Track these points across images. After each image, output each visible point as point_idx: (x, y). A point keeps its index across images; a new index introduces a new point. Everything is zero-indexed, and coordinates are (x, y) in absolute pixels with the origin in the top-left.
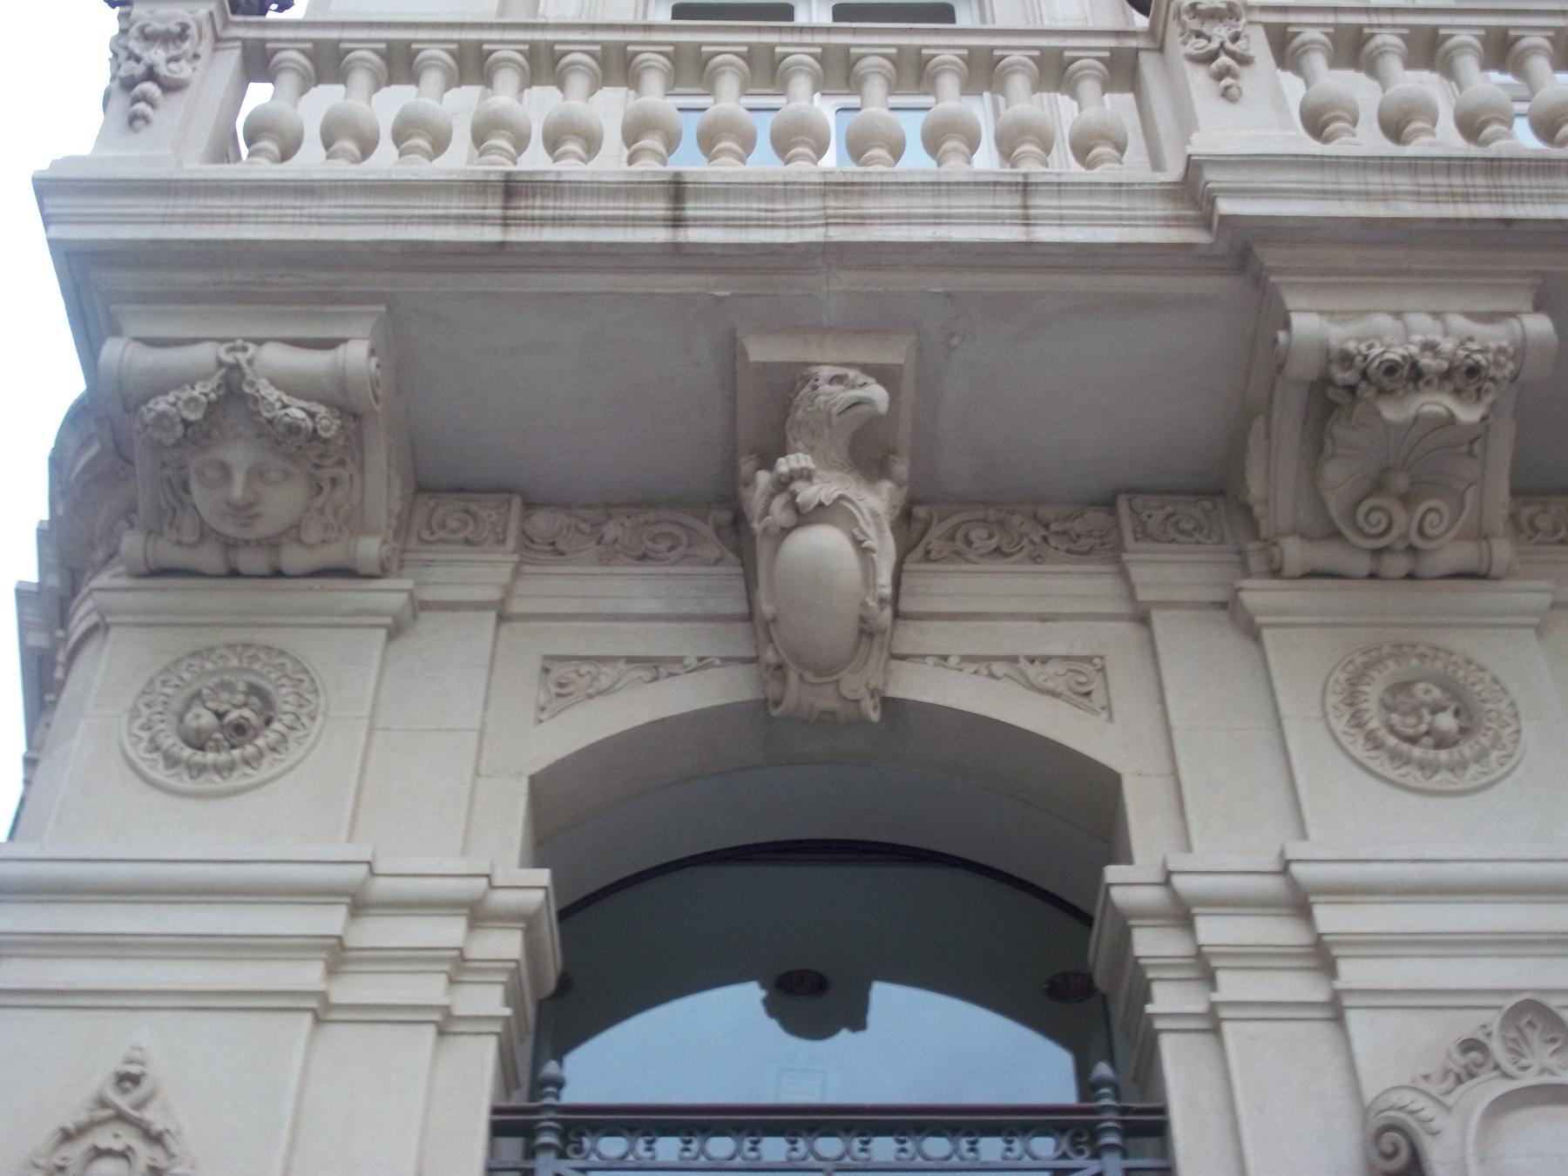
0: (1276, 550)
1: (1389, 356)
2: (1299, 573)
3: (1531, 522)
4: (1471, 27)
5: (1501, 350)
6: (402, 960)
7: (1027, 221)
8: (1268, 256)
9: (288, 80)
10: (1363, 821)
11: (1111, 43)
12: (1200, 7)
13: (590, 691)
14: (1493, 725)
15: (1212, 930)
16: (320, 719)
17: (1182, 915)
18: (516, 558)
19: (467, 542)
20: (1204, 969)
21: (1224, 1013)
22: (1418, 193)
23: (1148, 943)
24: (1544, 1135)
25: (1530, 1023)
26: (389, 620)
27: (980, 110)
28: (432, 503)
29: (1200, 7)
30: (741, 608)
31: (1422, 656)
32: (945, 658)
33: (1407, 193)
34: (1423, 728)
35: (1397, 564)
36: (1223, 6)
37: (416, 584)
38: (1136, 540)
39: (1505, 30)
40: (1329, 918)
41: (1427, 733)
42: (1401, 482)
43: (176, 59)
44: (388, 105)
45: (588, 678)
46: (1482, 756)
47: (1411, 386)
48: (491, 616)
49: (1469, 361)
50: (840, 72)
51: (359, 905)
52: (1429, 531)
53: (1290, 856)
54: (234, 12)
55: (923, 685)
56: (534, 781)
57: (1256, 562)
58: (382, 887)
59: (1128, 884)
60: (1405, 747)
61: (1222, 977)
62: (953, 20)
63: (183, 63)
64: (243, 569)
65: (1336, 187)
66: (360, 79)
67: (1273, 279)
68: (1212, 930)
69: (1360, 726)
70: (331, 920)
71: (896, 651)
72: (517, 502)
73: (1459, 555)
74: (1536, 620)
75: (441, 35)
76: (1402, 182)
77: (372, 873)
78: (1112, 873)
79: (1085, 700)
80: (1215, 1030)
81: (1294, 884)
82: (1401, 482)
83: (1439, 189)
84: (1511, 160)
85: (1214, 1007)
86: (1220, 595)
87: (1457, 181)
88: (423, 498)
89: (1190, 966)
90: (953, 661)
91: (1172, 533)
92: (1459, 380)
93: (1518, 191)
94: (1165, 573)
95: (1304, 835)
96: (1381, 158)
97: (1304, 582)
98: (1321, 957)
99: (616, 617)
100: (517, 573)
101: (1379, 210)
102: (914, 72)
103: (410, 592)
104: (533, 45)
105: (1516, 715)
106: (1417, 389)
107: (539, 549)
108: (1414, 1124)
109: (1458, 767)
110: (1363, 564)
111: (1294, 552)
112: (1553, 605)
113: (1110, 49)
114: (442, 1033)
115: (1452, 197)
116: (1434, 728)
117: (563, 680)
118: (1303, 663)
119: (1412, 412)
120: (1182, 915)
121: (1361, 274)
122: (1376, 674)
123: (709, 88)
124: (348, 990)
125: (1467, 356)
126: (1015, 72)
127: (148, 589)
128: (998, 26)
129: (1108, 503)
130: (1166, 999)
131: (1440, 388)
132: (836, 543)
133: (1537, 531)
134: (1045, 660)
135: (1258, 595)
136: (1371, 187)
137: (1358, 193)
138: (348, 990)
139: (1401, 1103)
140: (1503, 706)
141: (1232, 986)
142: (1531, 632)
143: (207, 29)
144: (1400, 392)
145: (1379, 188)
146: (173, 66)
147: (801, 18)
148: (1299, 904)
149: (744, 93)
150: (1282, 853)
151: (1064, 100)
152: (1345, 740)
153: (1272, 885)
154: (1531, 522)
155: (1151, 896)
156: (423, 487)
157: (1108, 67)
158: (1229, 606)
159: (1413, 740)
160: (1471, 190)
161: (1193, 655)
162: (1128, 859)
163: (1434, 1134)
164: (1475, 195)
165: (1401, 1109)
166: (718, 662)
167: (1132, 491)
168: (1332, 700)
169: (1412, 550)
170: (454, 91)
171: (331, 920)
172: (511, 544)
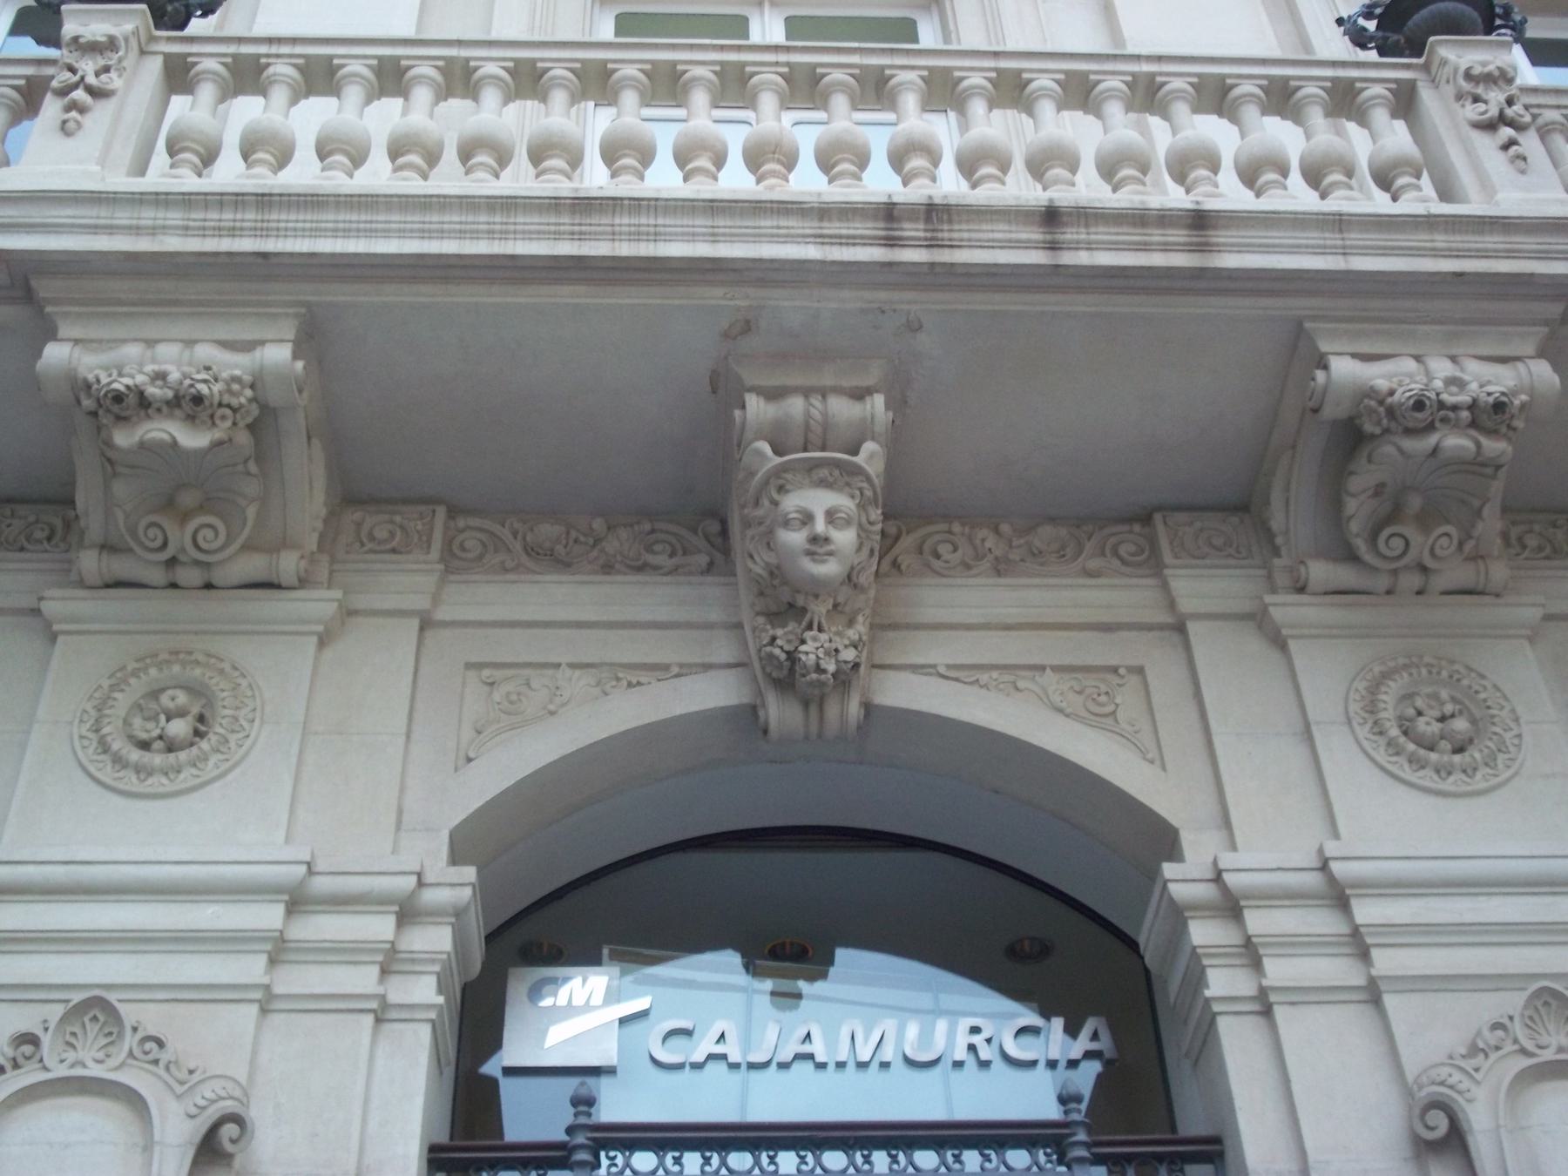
0: (1302, 569)
1: (115, 386)
3: (1520, 539)
4: (365, 57)
5: (236, 379)
6: (1309, 944)
7: (1053, 247)
8: (44, 288)
9: (280, 95)
10: (1389, 821)
11: (29, 71)
12: (82, 40)
14: (1497, 729)
19: (394, 551)
20: (1251, 954)
21: (1273, 998)
22: (187, 228)
23: (1203, 933)
24: (1562, 1109)
25: (1546, 1003)
26: (320, 628)
27: (943, 130)
28: (357, 516)
29: (82, 40)
31: (159, 666)
33: (176, 227)
34: (156, 732)
35: (1412, 580)
36: (103, 39)
39: (396, 60)
40: (1367, 912)
41: (160, 737)
42: (1415, 503)
43: (107, 69)
44: (384, 118)
46: (1490, 762)
47: (142, 413)
48: (415, 623)
49: (193, 390)
50: (805, 88)
51: (297, 902)
52: (1438, 551)
54: (157, 27)
55: (901, 692)
57: (1282, 579)
58: (321, 885)
59: (1183, 879)
60: (1422, 752)
61: (1268, 963)
62: (915, 40)
63: (113, 74)
64: (181, 582)
65: (109, 222)
66: (353, 93)
67: (49, 309)
68: (1258, 921)
70: (270, 916)
71: (877, 661)
72: (441, 512)
73: (1461, 574)
74: (1529, 632)
75: (495, 53)
76: (175, 217)
78: (1169, 869)
80: (1267, 1012)
81: (1332, 880)
82: (1415, 503)
83: (223, 224)
84: (281, 195)
85: (1263, 993)
86: (1246, 606)
87: (228, 215)
88: (353, 515)
89: (1240, 955)
92: (187, 406)
93: (282, 225)
94: (1199, 588)
95: (1233, 847)
96: (157, 194)
97: (1328, 599)
98: (1359, 945)
99: (986, 626)
100: (443, 581)
101: (143, 245)
102: (875, 90)
104: (450, 60)
105: (1517, 720)
106: (148, 417)
107: (454, 562)
108: (1455, 1095)
109: (1469, 771)
110: (1383, 582)
111: (1320, 572)
112: (1548, 618)
113: (28, 78)
115: (219, 231)
116: (1443, 738)
118: (1327, 676)
119: (137, 438)
120: (1231, 907)
121: (133, 304)
122: (1391, 683)
123: (750, 102)
125: (192, 386)
126: (973, 94)
128: (964, 46)
130: (1222, 982)
131: (171, 416)
133: (1524, 547)
135: (1287, 610)
136: (143, 222)
137: (130, 227)
139: (1438, 1079)
140: (1504, 713)
141: (1277, 971)
142: (1526, 643)
143: (134, 43)
144: (135, 419)
145: (150, 222)
146: (103, 77)
147: (755, 37)
148: (1339, 897)
149: (855, 108)
151: (1155, 121)
152: (1366, 744)
154: (1520, 539)
155: (1205, 892)
157: (994, 86)
158: (1258, 619)
159: (145, 745)
160: (238, 224)
161: (1228, 666)
163: (1469, 1101)
164: (242, 229)
165: (1442, 1083)
167: (1160, 508)
168: (1354, 707)
169: (1424, 569)
170: (442, 104)
171: (270, 916)
172: (435, 554)
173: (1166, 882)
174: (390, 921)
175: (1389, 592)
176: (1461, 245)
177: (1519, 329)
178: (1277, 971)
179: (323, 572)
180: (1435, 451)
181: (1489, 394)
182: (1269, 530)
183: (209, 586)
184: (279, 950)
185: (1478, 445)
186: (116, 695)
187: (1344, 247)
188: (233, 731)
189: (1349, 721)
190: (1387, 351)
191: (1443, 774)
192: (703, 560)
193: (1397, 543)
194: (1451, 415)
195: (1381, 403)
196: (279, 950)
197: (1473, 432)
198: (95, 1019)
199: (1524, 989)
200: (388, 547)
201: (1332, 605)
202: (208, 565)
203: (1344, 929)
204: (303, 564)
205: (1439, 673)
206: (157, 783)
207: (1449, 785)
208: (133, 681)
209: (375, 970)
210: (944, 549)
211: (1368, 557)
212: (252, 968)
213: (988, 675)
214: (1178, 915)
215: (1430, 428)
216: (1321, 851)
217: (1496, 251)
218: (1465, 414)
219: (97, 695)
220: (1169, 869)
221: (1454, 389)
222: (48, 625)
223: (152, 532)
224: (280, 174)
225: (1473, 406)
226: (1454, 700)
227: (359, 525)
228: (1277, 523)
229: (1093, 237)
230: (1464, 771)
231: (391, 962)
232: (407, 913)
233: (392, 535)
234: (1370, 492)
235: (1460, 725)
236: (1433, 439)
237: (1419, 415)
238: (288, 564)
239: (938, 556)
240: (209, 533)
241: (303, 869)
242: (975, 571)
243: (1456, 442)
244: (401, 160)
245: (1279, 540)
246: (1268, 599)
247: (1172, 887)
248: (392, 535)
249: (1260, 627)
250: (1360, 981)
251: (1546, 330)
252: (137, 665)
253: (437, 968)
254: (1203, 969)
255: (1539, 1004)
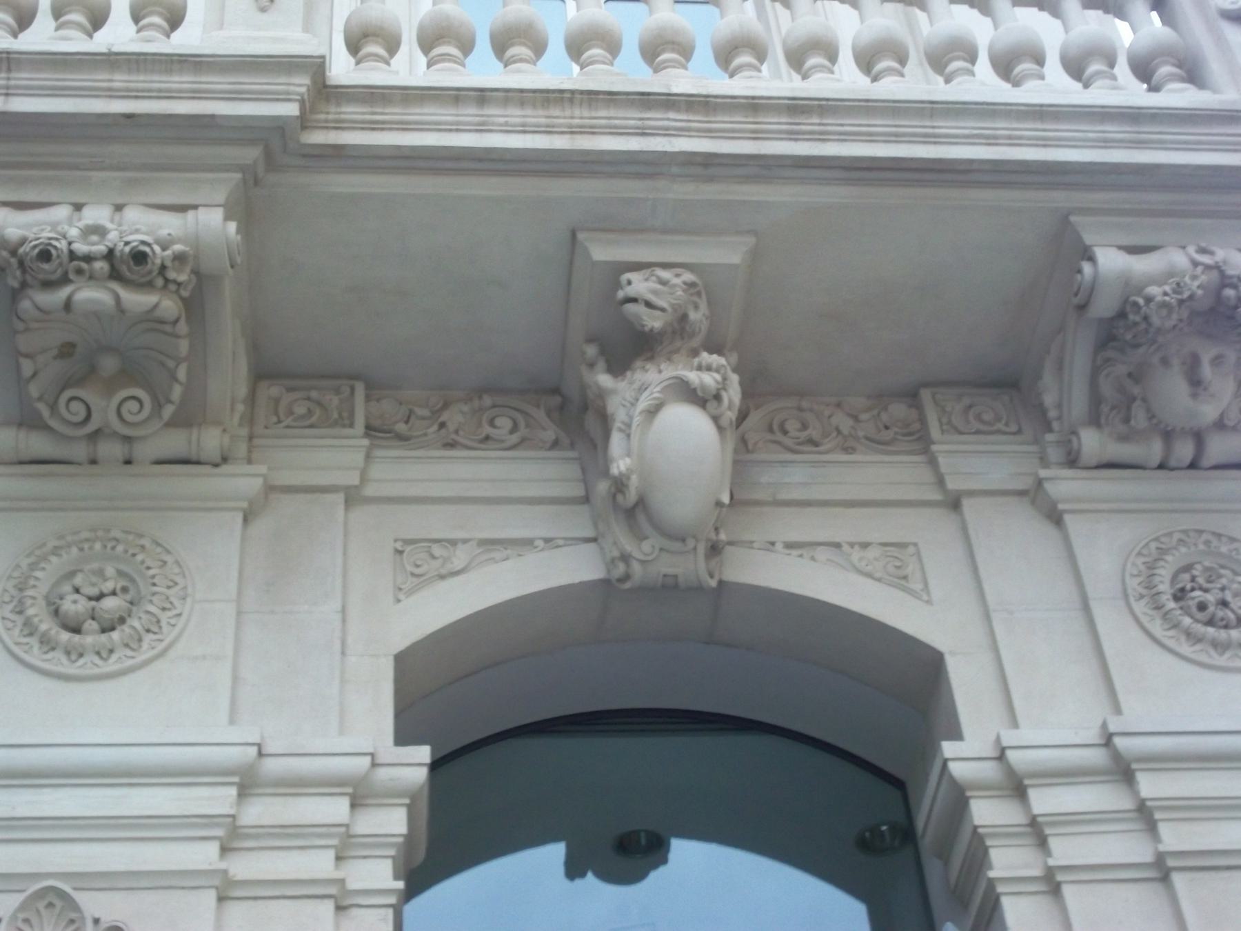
2: (1094, 462)
13: (443, 571)
15: (1044, 801)
16: (189, 600)
17: (1016, 787)
18: (366, 442)
20: (1037, 833)
23: (986, 812)
28: (275, 391)
30: (578, 491)
32: (773, 544)
37: (269, 469)
38: (943, 432)
40: (1150, 785)
45: (439, 562)
51: (248, 783)
53: (1005, 744)
56: (401, 660)
57: (1054, 454)
58: (272, 766)
59: (964, 757)
61: (1053, 843)
68: (1044, 801)
69: (1158, 608)
70: (220, 800)
77: (260, 754)
78: (949, 748)
79: (903, 582)
81: (1116, 756)
82: (109, 364)
88: (271, 390)
90: (779, 546)
91: (977, 425)
95: (1015, 724)
98: (1146, 817)
100: (368, 457)
103: (264, 476)
111: (1091, 442)
114: (340, 908)
117: (418, 562)
120: (1016, 787)
124: (243, 867)
127: (11, 475)
129: (911, 396)
130: (1006, 861)
132: (672, 434)
134: (865, 546)
135: (1065, 486)
138: (243, 867)
141: (1064, 850)
148: (1123, 771)
150: (998, 740)
152: (1144, 620)
153: (1097, 757)
155: (989, 771)
156: (261, 374)
162: (956, 735)
166: (540, 543)
171: (220, 800)
173: (945, 761)
174: (345, 803)
175: (1193, 465)
176: (141, 85)
177: (210, 176)
178: (1064, 850)
179: (242, 449)
180: (68, 305)
181: (127, 243)
182: (1041, 404)
183: (93, 462)
184: (233, 838)
185: (118, 299)
186: (38, 574)
187: (8, 88)
188: (164, 609)
189: (1126, 596)
190: (54, 200)
191: (74, 657)
192: (550, 434)
193: (78, 409)
194: (84, 265)
195: (14, 253)
196: (233, 838)
197: (115, 286)
198: (50, 905)
199: (23, 891)
200: (308, 423)
201: (24, 475)
202: (128, 439)
203: (1127, 803)
204: (226, 440)
205: (113, 548)
206: (89, 664)
207: (112, 665)
208: (54, 559)
209: (331, 854)
210: (792, 426)
211: (53, 423)
212: (204, 855)
213: (842, 554)
214: (959, 798)
215: (65, 280)
216: (1104, 725)
217: (180, 91)
218: (101, 266)
219: (16, 574)
220: (949, 748)
221: (95, 238)
222: (1053, 505)
223: (75, 406)
224: (99, 35)
225: (110, 255)
226: (121, 574)
227: (277, 401)
228: (1049, 400)
229: (12, 83)
230: (98, 653)
231: (346, 846)
232: (360, 795)
233: (310, 412)
234: (55, 352)
235: (110, 604)
236: (64, 292)
237: (46, 266)
238: (211, 441)
239: (785, 433)
240: (133, 405)
241: (253, 751)
242: (821, 448)
243: (90, 295)
244: (142, 23)
245: (1052, 414)
246: (1043, 473)
247: (952, 766)
248: (310, 412)
249: (1033, 502)
250: (1149, 858)
251: (239, 176)
252: (57, 543)
253: (392, 852)
254: (986, 851)
255: (41, 905)
